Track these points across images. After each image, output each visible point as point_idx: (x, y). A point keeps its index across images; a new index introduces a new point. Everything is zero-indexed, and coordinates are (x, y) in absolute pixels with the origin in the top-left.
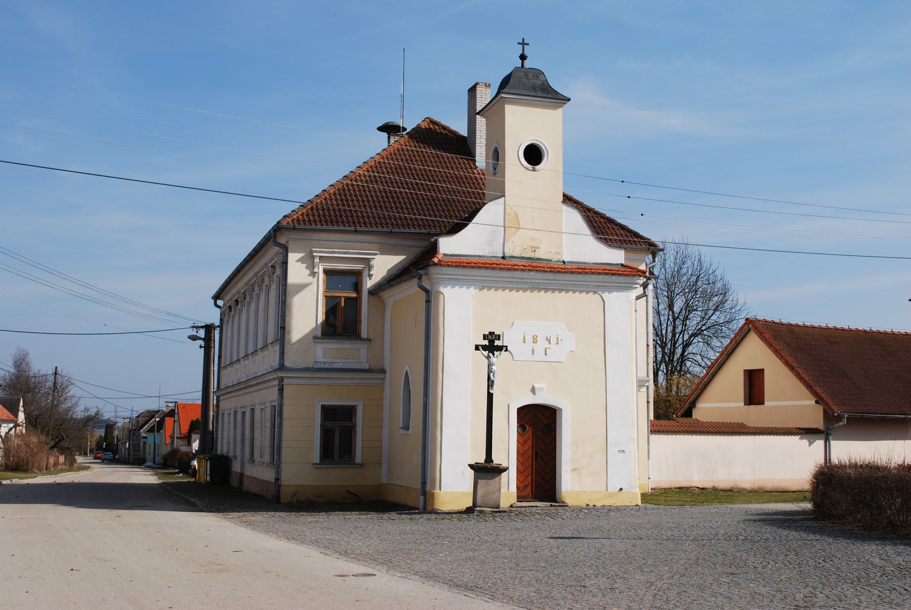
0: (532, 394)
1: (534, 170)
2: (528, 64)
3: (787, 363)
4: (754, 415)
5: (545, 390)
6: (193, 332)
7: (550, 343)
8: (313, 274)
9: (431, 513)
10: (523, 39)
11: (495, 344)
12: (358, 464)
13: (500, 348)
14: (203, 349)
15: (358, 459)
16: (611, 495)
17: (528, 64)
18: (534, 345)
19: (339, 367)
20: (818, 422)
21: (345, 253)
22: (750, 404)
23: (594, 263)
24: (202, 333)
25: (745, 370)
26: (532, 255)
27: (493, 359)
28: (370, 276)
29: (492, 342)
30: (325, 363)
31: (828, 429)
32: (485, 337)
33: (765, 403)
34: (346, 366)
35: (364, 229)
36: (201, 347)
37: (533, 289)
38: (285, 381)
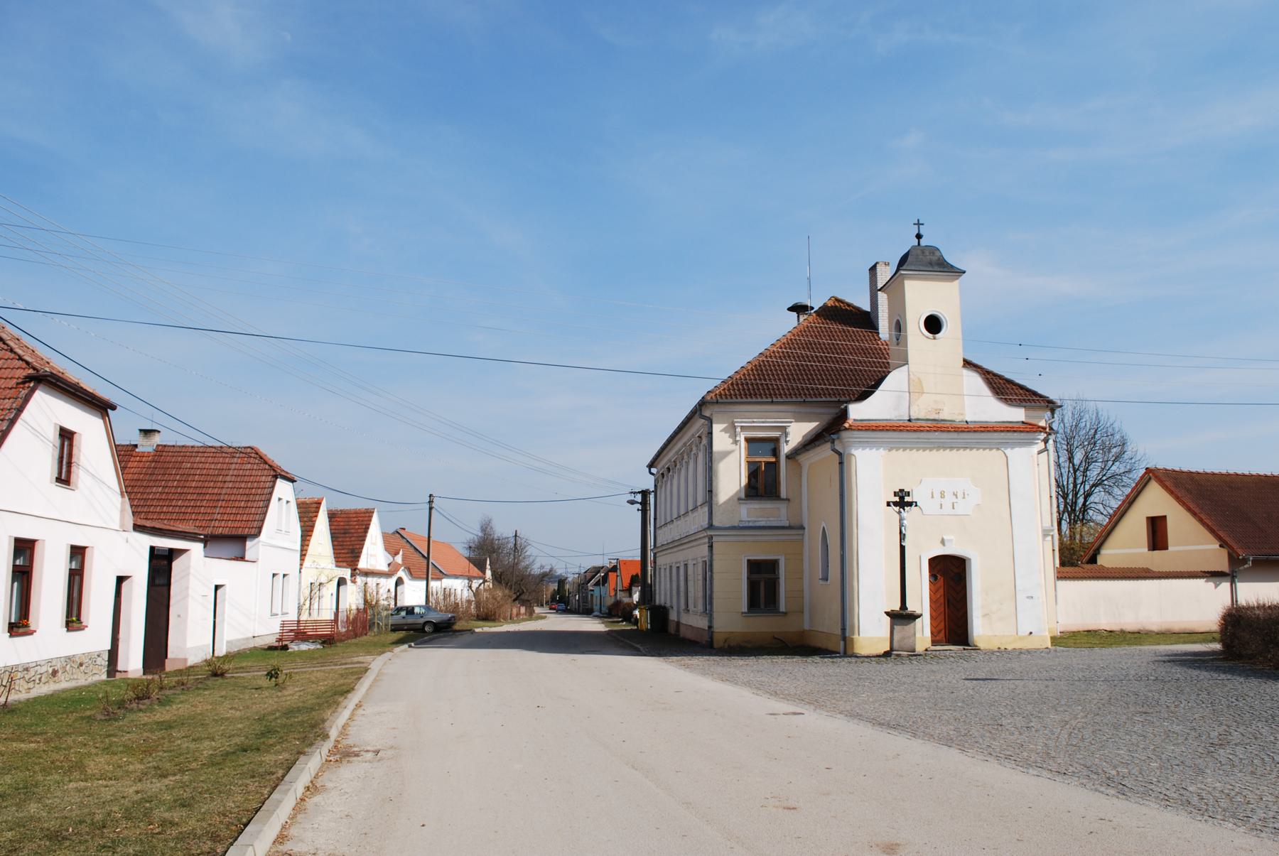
0: (941, 545)
1: (934, 338)
2: (924, 242)
4: (1158, 560)
6: (631, 497)
7: (957, 498)
8: (736, 442)
9: (851, 656)
10: (918, 220)
11: (906, 500)
12: (783, 613)
13: (910, 504)
14: (640, 512)
15: (782, 608)
16: (1022, 638)
18: (942, 500)
19: (762, 525)
20: (1223, 565)
21: (763, 422)
23: (996, 422)
24: (639, 498)
25: (1148, 518)
26: (936, 417)
27: (904, 514)
28: (787, 442)
29: (902, 498)
30: (749, 521)
31: (1233, 572)
32: (895, 494)
34: (769, 524)
36: (638, 510)
37: (938, 448)
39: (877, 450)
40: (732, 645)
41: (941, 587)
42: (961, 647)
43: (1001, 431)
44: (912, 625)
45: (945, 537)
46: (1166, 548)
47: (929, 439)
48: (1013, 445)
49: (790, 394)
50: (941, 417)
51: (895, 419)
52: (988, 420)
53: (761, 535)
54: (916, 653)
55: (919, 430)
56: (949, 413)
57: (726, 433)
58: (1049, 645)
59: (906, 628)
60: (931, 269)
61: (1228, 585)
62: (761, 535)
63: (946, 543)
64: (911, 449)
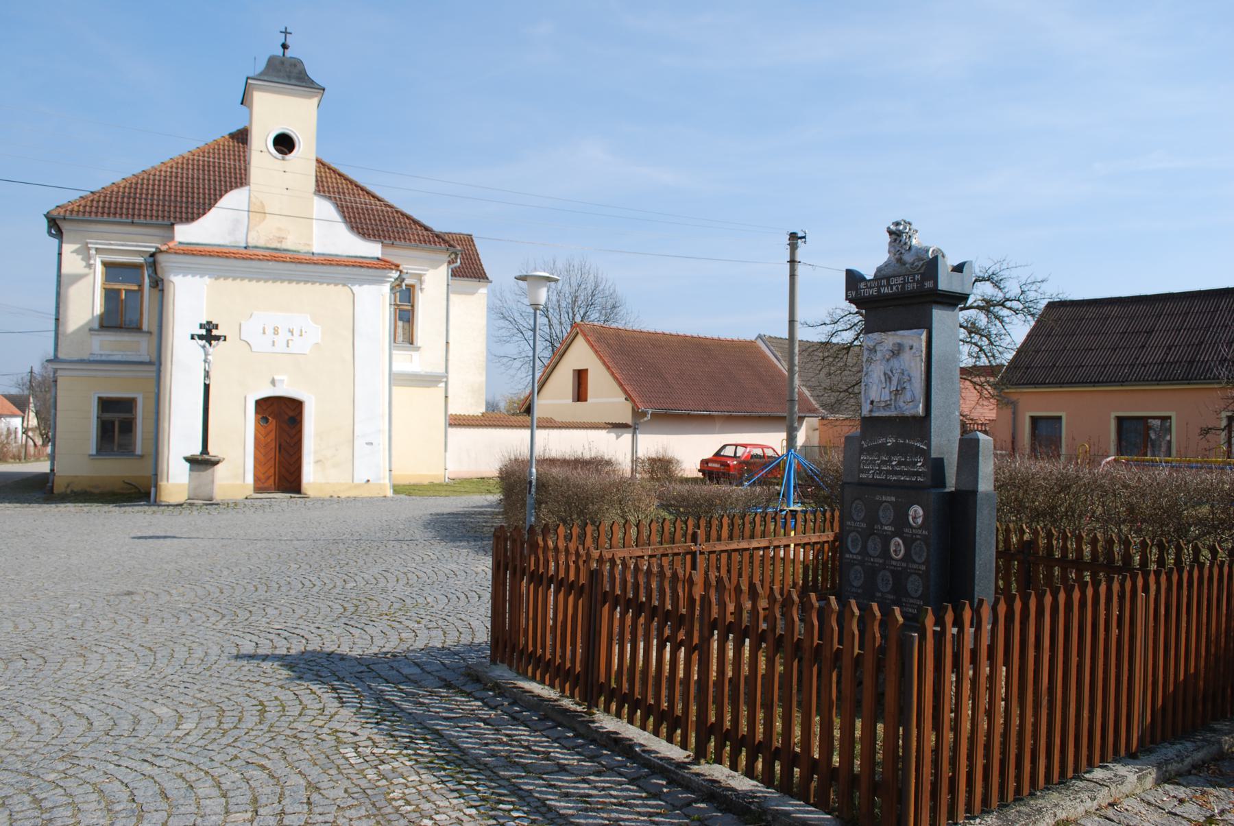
0: (271, 386)
1: (283, 159)
2: (289, 53)
3: (605, 363)
4: (581, 411)
5: (285, 382)
7: (293, 335)
8: (89, 266)
9: (159, 505)
10: (286, 28)
11: (213, 334)
12: (138, 456)
13: (217, 338)
15: (139, 451)
16: (358, 486)
17: (289, 53)
18: (275, 336)
20: (628, 419)
21: (123, 245)
22: (578, 401)
23: (347, 256)
25: (574, 370)
26: (278, 246)
27: (211, 350)
29: (209, 331)
30: (101, 355)
31: (635, 424)
32: (202, 326)
33: (589, 399)
34: (125, 359)
35: (142, 220)
37: (275, 280)
38: (59, 373)
39: (201, 277)
40: (75, 490)
41: (271, 431)
42: (288, 495)
43: (346, 265)
44: (210, 471)
45: (276, 378)
46: (586, 400)
47: (263, 269)
48: (362, 282)
49: (430, 242)
50: (284, 246)
51: (228, 244)
52: (339, 253)
53: (116, 371)
54: (214, 502)
55: (250, 258)
56: (292, 242)
57: (78, 254)
58: (390, 493)
59: (204, 474)
60: (287, 82)
61: (629, 436)
62: (116, 371)
63: (277, 384)
64: (242, 279)
